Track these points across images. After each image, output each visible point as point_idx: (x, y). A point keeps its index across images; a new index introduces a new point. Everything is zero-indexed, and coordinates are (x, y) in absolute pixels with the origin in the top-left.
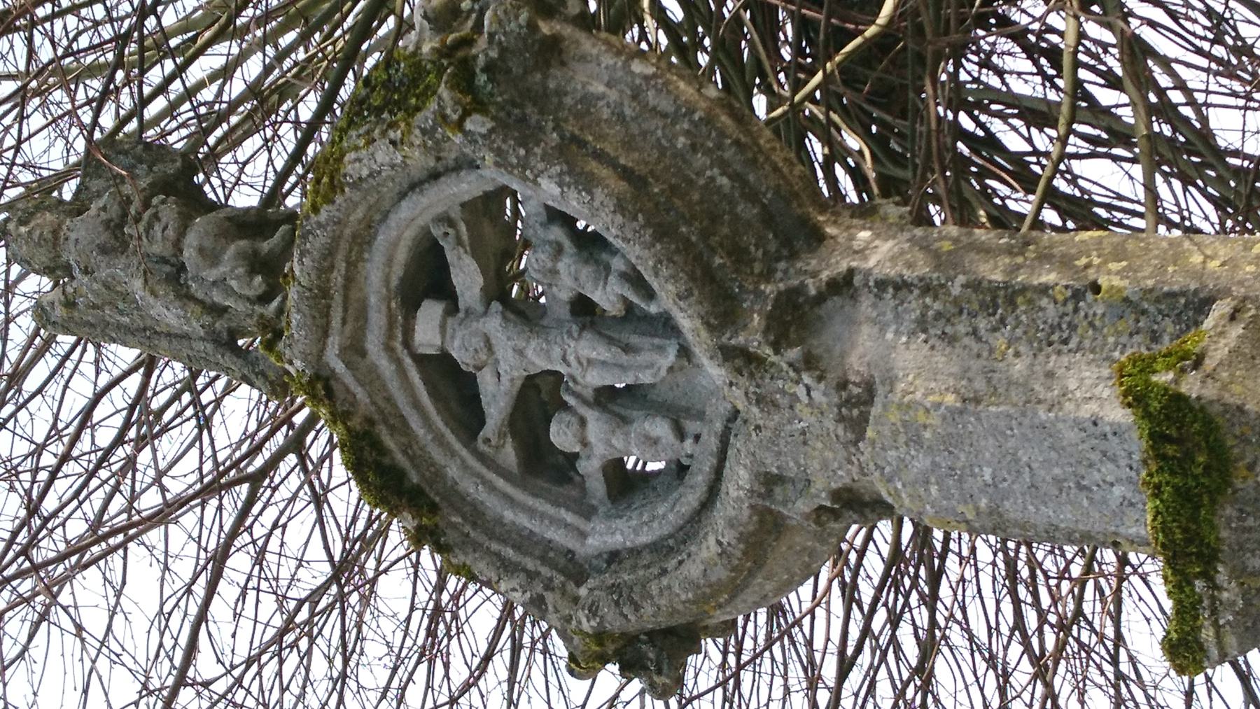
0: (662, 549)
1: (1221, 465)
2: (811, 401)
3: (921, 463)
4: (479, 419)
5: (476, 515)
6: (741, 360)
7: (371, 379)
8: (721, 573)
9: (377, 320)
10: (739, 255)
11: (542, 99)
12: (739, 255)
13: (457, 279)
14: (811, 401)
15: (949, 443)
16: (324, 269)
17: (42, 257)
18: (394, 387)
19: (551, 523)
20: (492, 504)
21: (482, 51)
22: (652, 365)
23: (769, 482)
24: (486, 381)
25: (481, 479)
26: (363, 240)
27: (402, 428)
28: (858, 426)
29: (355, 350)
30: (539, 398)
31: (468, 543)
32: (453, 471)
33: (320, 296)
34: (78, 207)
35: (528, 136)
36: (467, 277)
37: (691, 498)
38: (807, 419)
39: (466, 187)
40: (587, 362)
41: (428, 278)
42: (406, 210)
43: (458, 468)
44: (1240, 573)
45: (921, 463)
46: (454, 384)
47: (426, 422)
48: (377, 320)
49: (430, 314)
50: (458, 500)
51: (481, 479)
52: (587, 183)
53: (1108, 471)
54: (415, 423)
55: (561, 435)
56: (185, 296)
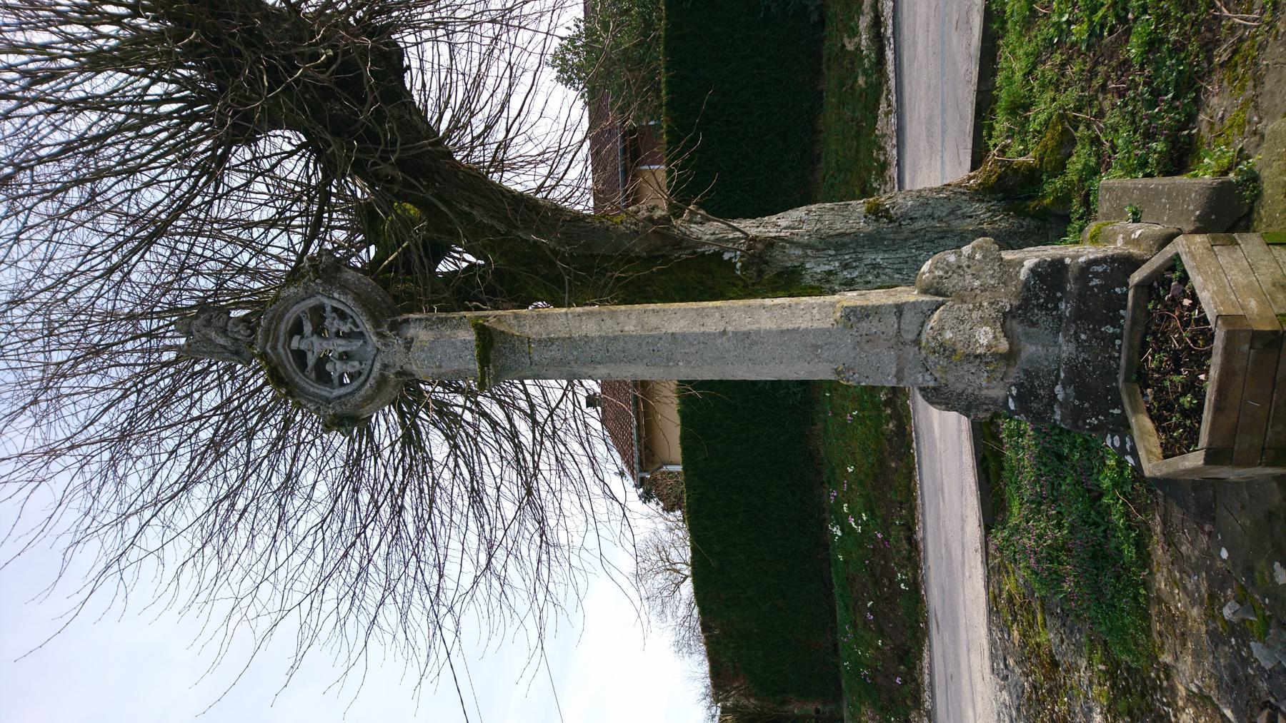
0: (352, 393)
1: (491, 341)
2: (398, 343)
3: (424, 355)
4: (306, 365)
5: (302, 390)
6: (381, 335)
7: (278, 355)
8: (370, 392)
9: (282, 339)
10: (382, 314)
11: (335, 278)
12: (382, 314)
13: (306, 329)
14: (398, 343)
15: (430, 350)
16: (270, 323)
17: (185, 329)
18: (284, 357)
19: (324, 391)
20: (307, 387)
21: (321, 266)
22: (355, 345)
23: (385, 366)
24: (309, 355)
25: (307, 383)
26: (281, 318)
27: (284, 367)
28: (408, 349)
29: (274, 348)
30: (322, 361)
31: (299, 396)
32: (297, 380)
33: (267, 331)
34: (196, 317)
35: (331, 284)
36: (308, 328)
37: (363, 378)
38: (396, 347)
39: (312, 302)
40: (341, 346)
41: (297, 329)
42: (295, 308)
43: (299, 379)
44: (494, 366)
45: (424, 355)
46: (300, 356)
47: (291, 366)
48: (282, 339)
49: (296, 339)
50: (296, 385)
51: (307, 383)
52: (346, 294)
53: (467, 352)
54: (288, 367)
55: (329, 367)
56: (227, 336)
